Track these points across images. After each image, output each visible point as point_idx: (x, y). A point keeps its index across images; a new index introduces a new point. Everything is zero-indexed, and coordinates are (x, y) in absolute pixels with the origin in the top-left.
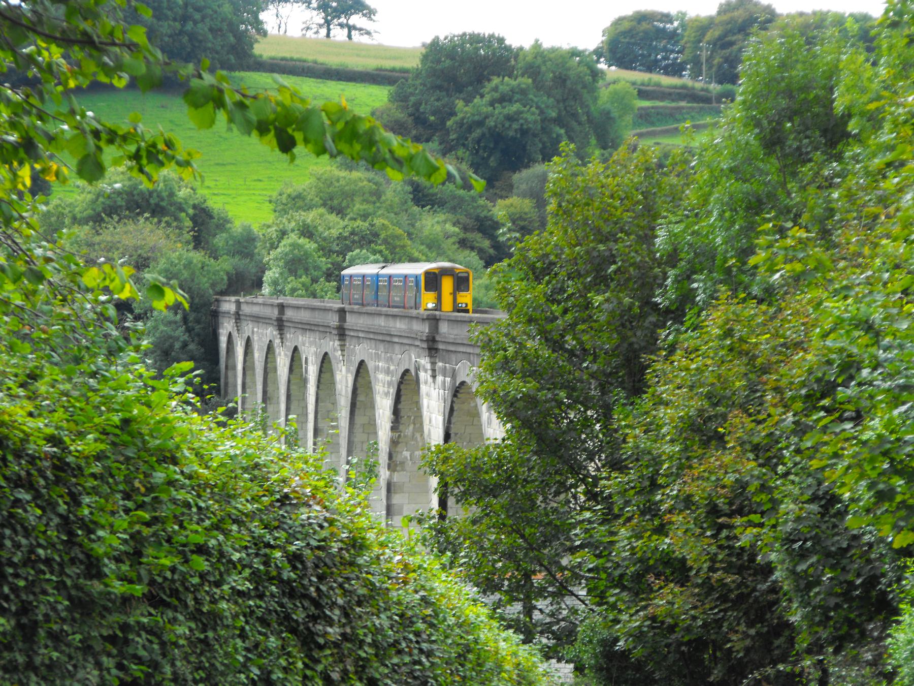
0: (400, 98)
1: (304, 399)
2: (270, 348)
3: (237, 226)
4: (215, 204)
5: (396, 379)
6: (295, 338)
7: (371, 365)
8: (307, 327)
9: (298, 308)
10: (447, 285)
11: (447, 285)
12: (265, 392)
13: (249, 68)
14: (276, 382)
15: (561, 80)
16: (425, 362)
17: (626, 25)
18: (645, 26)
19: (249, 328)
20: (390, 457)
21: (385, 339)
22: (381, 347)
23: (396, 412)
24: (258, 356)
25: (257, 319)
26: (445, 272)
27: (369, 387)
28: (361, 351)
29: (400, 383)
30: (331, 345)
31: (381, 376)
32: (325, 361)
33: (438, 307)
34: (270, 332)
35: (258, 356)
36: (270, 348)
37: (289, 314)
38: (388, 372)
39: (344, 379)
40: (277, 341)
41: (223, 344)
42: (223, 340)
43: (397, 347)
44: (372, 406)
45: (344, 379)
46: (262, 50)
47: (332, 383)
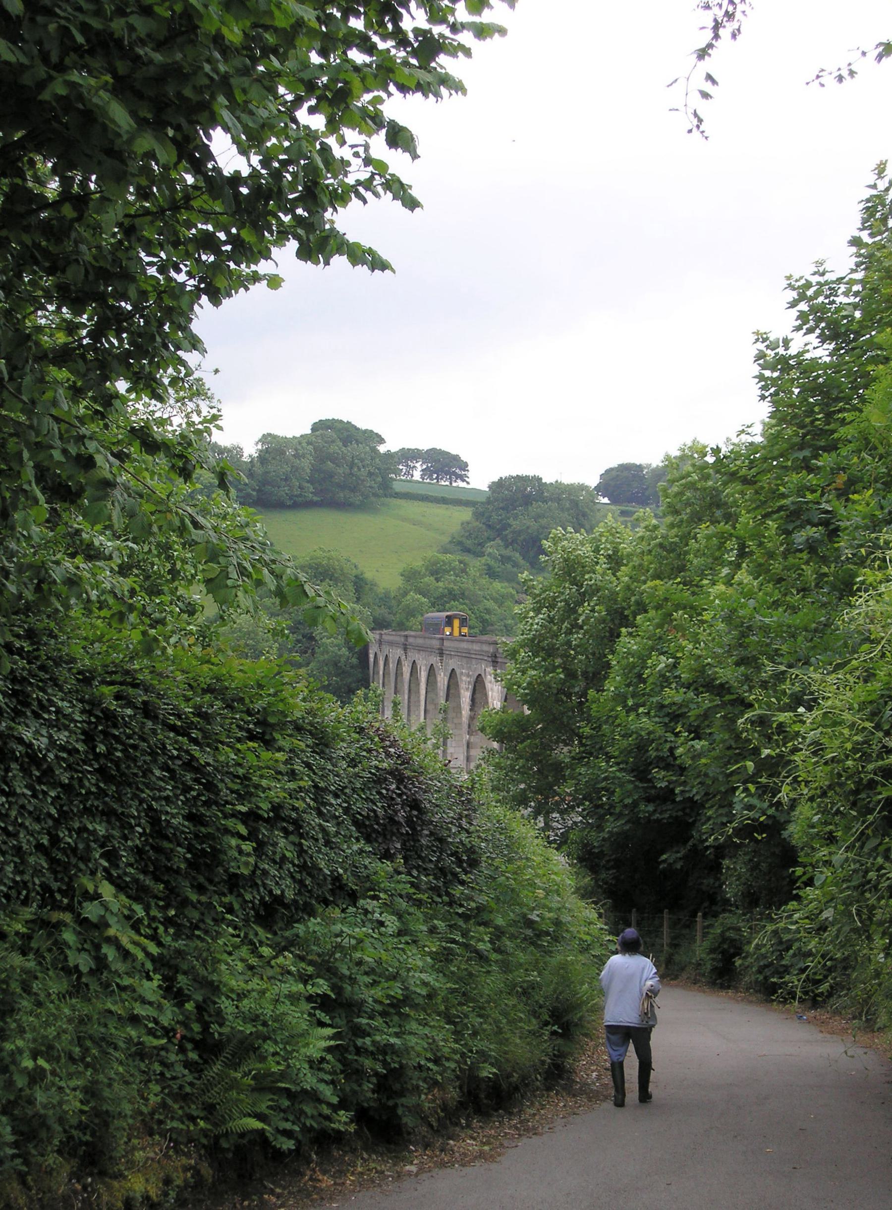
0: (477, 515)
1: (418, 692)
2: (399, 661)
3: (380, 590)
4: (369, 575)
5: (473, 680)
6: (414, 655)
7: (458, 671)
8: (420, 649)
9: (415, 637)
10: (456, 623)
11: (456, 623)
12: (396, 688)
13: (391, 496)
14: (402, 682)
15: (575, 504)
16: (490, 670)
17: (614, 473)
18: (626, 473)
19: (386, 649)
20: (469, 726)
21: (467, 656)
22: (465, 660)
23: (473, 700)
24: (392, 666)
25: (391, 644)
26: (455, 616)
27: (457, 685)
28: (453, 663)
29: (476, 682)
30: (434, 660)
31: (464, 678)
32: (431, 671)
33: (451, 634)
34: (399, 652)
35: (392, 666)
36: (399, 661)
37: (411, 640)
38: (468, 676)
39: (442, 680)
40: (403, 657)
41: (372, 659)
42: (372, 656)
43: (474, 661)
44: (458, 696)
45: (442, 680)
46: (397, 487)
47: (436, 682)
